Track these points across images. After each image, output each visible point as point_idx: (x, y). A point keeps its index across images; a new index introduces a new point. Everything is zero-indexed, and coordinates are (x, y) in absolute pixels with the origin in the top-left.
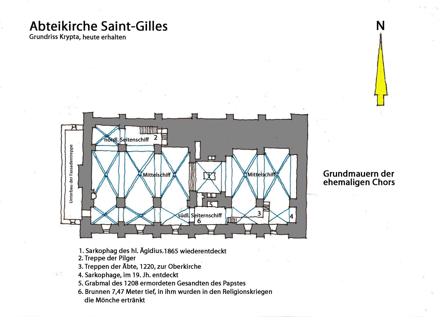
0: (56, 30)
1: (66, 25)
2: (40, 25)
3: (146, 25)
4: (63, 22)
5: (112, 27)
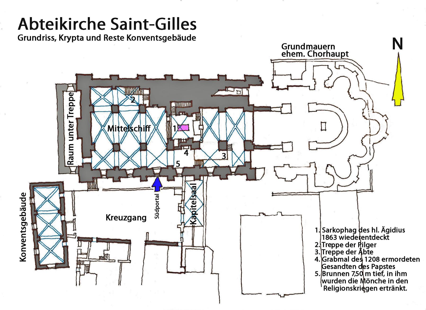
0: (52, 29)
1: (65, 22)
2: (31, 22)
3: (169, 22)
4: (61, 18)
5: (124, 26)
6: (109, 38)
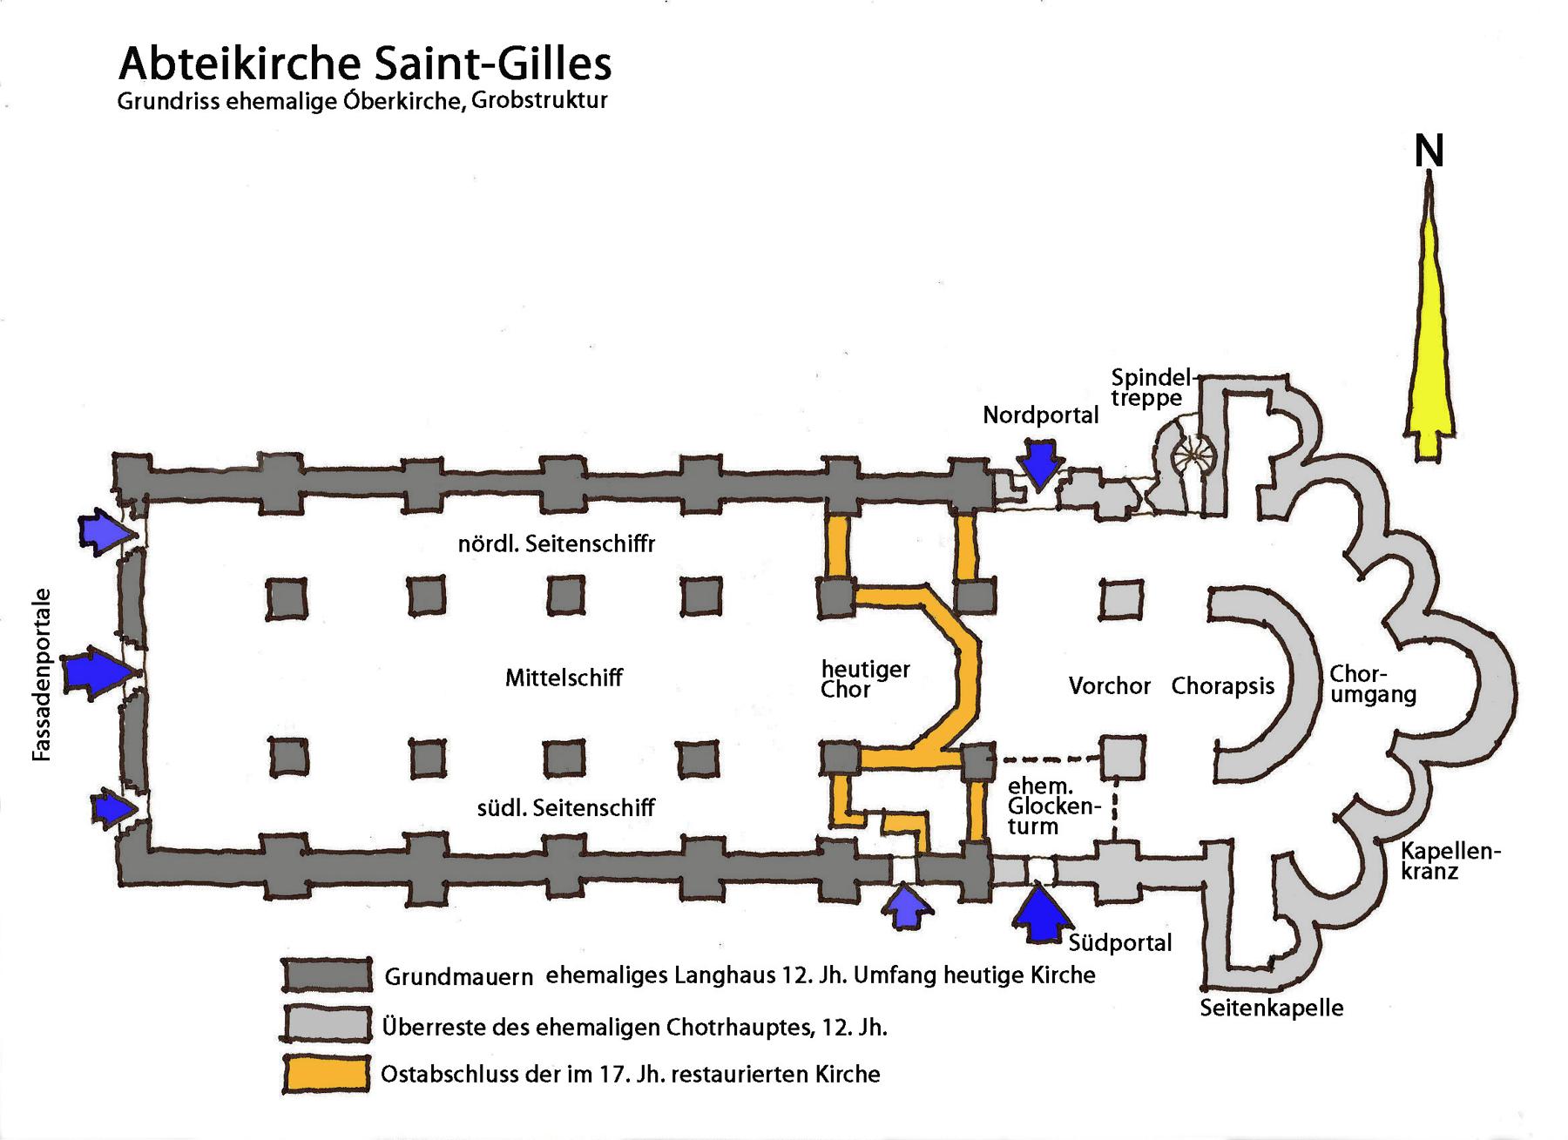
1: (250, 58)
2: (155, 59)
3: (535, 59)
4: (238, 47)
5: (413, 67)
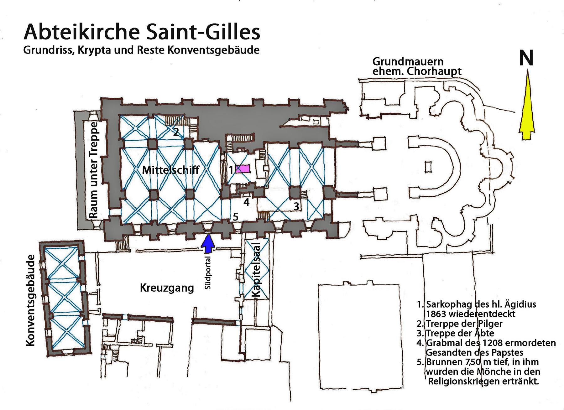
0: (69, 38)
1: (87, 29)
2: (41, 30)
3: (224, 30)
4: (81, 24)
5: (165, 34)
6: (145, 51)
